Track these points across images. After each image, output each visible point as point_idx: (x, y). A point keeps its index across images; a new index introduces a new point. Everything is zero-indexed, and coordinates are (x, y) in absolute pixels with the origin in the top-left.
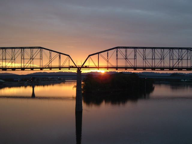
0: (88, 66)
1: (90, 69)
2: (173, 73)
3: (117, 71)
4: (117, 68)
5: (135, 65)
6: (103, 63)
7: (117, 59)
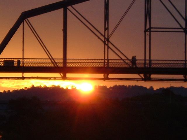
0: (19, 62)
1: (26, 75)
2: (169, 86)
3: (147, 85)
4: (147, 71)
5: (147, 58)
6: (85, 48)
7: (148, 30)
